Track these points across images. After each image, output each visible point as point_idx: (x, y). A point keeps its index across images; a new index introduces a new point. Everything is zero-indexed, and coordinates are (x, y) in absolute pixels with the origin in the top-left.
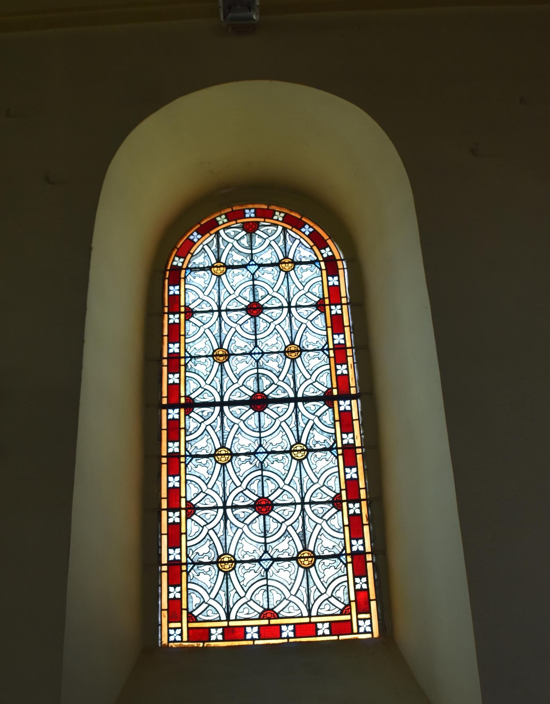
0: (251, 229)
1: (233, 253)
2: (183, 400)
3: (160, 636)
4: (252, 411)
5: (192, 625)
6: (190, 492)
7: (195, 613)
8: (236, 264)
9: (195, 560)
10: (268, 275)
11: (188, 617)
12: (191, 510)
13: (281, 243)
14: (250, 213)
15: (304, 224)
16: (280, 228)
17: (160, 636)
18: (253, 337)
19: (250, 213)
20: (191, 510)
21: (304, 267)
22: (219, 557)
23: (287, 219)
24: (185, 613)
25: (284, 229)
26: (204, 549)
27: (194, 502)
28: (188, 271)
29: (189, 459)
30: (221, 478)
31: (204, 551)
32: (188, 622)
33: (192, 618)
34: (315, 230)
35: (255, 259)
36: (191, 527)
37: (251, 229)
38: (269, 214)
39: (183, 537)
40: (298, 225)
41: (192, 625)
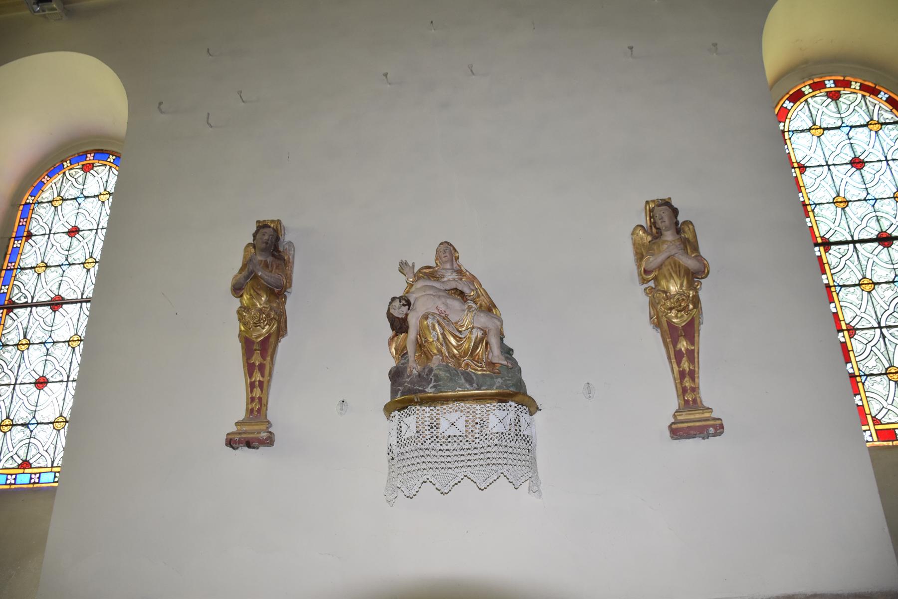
0: (834, 96)
1: (882, 112)
2: (819, 240)
3: (698, 424)
4: (881, 247)
5: (878, 427)
6: (847, 316)
7: (879, 417)
8: (887, 121)
9: (867, 373)
10: (861, 135)
11: (873, 421)
12: (852, 331)
13: (864, 108)
14: (830, 84)
15: (879, 92)
16: (860, 96)
17: (698, 424)
18: (80, 211)
19: (830, 84)
20: (852, 331)
21: (890, 127)
22: (887, 369)
23: (863, 88)
24: (869, 417)
25: (864, 96)
26: (872, 363)
27: (853, 324)
28: (791, 133)
29: (838, 289)
30: (870, 303)
31: (872, 365)
32: (874, 425)
33: (876, 421)
34: (890, 97)
35: (845, 120)
36: (856, 345)
37: (834, 96)
38: (847, 84)
39: (851, 353)
40: (875, 92)
41: (878, 427)
